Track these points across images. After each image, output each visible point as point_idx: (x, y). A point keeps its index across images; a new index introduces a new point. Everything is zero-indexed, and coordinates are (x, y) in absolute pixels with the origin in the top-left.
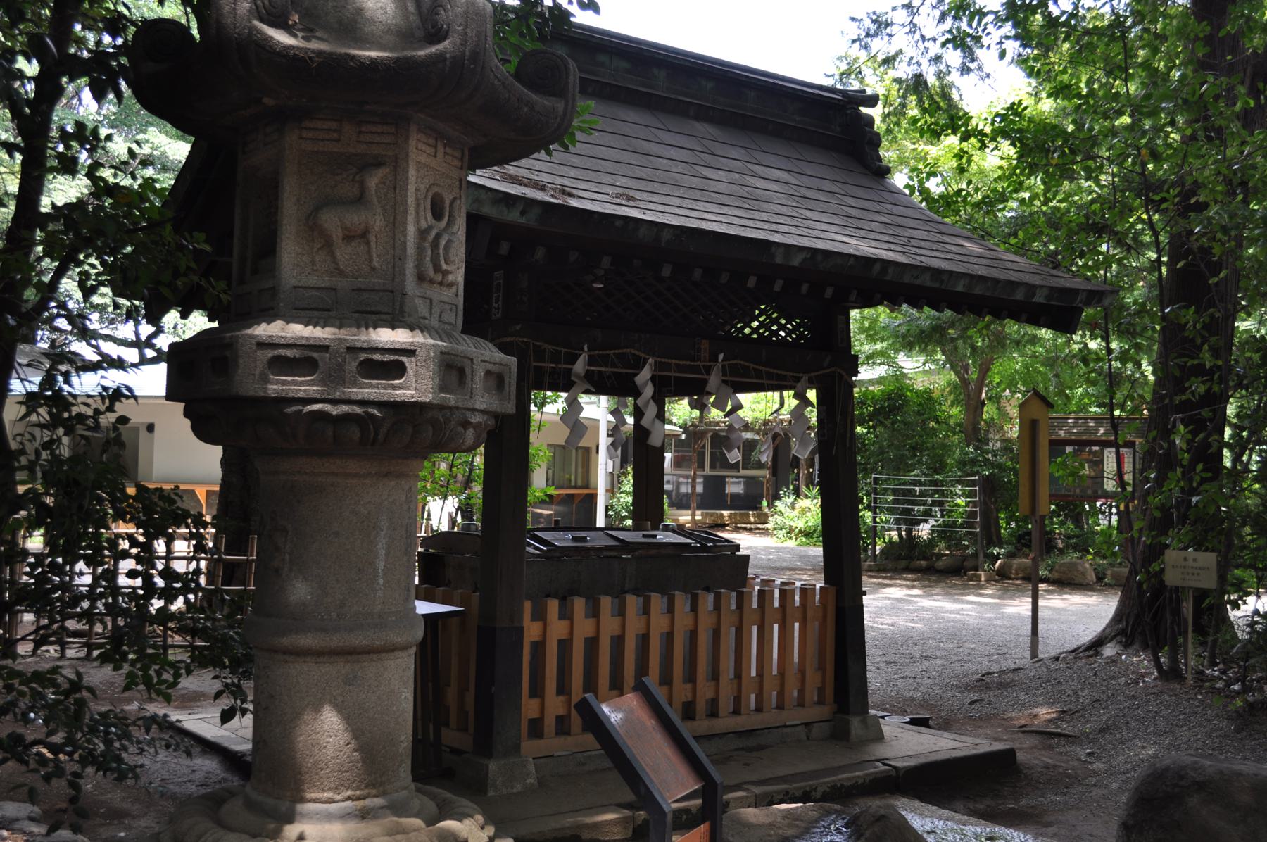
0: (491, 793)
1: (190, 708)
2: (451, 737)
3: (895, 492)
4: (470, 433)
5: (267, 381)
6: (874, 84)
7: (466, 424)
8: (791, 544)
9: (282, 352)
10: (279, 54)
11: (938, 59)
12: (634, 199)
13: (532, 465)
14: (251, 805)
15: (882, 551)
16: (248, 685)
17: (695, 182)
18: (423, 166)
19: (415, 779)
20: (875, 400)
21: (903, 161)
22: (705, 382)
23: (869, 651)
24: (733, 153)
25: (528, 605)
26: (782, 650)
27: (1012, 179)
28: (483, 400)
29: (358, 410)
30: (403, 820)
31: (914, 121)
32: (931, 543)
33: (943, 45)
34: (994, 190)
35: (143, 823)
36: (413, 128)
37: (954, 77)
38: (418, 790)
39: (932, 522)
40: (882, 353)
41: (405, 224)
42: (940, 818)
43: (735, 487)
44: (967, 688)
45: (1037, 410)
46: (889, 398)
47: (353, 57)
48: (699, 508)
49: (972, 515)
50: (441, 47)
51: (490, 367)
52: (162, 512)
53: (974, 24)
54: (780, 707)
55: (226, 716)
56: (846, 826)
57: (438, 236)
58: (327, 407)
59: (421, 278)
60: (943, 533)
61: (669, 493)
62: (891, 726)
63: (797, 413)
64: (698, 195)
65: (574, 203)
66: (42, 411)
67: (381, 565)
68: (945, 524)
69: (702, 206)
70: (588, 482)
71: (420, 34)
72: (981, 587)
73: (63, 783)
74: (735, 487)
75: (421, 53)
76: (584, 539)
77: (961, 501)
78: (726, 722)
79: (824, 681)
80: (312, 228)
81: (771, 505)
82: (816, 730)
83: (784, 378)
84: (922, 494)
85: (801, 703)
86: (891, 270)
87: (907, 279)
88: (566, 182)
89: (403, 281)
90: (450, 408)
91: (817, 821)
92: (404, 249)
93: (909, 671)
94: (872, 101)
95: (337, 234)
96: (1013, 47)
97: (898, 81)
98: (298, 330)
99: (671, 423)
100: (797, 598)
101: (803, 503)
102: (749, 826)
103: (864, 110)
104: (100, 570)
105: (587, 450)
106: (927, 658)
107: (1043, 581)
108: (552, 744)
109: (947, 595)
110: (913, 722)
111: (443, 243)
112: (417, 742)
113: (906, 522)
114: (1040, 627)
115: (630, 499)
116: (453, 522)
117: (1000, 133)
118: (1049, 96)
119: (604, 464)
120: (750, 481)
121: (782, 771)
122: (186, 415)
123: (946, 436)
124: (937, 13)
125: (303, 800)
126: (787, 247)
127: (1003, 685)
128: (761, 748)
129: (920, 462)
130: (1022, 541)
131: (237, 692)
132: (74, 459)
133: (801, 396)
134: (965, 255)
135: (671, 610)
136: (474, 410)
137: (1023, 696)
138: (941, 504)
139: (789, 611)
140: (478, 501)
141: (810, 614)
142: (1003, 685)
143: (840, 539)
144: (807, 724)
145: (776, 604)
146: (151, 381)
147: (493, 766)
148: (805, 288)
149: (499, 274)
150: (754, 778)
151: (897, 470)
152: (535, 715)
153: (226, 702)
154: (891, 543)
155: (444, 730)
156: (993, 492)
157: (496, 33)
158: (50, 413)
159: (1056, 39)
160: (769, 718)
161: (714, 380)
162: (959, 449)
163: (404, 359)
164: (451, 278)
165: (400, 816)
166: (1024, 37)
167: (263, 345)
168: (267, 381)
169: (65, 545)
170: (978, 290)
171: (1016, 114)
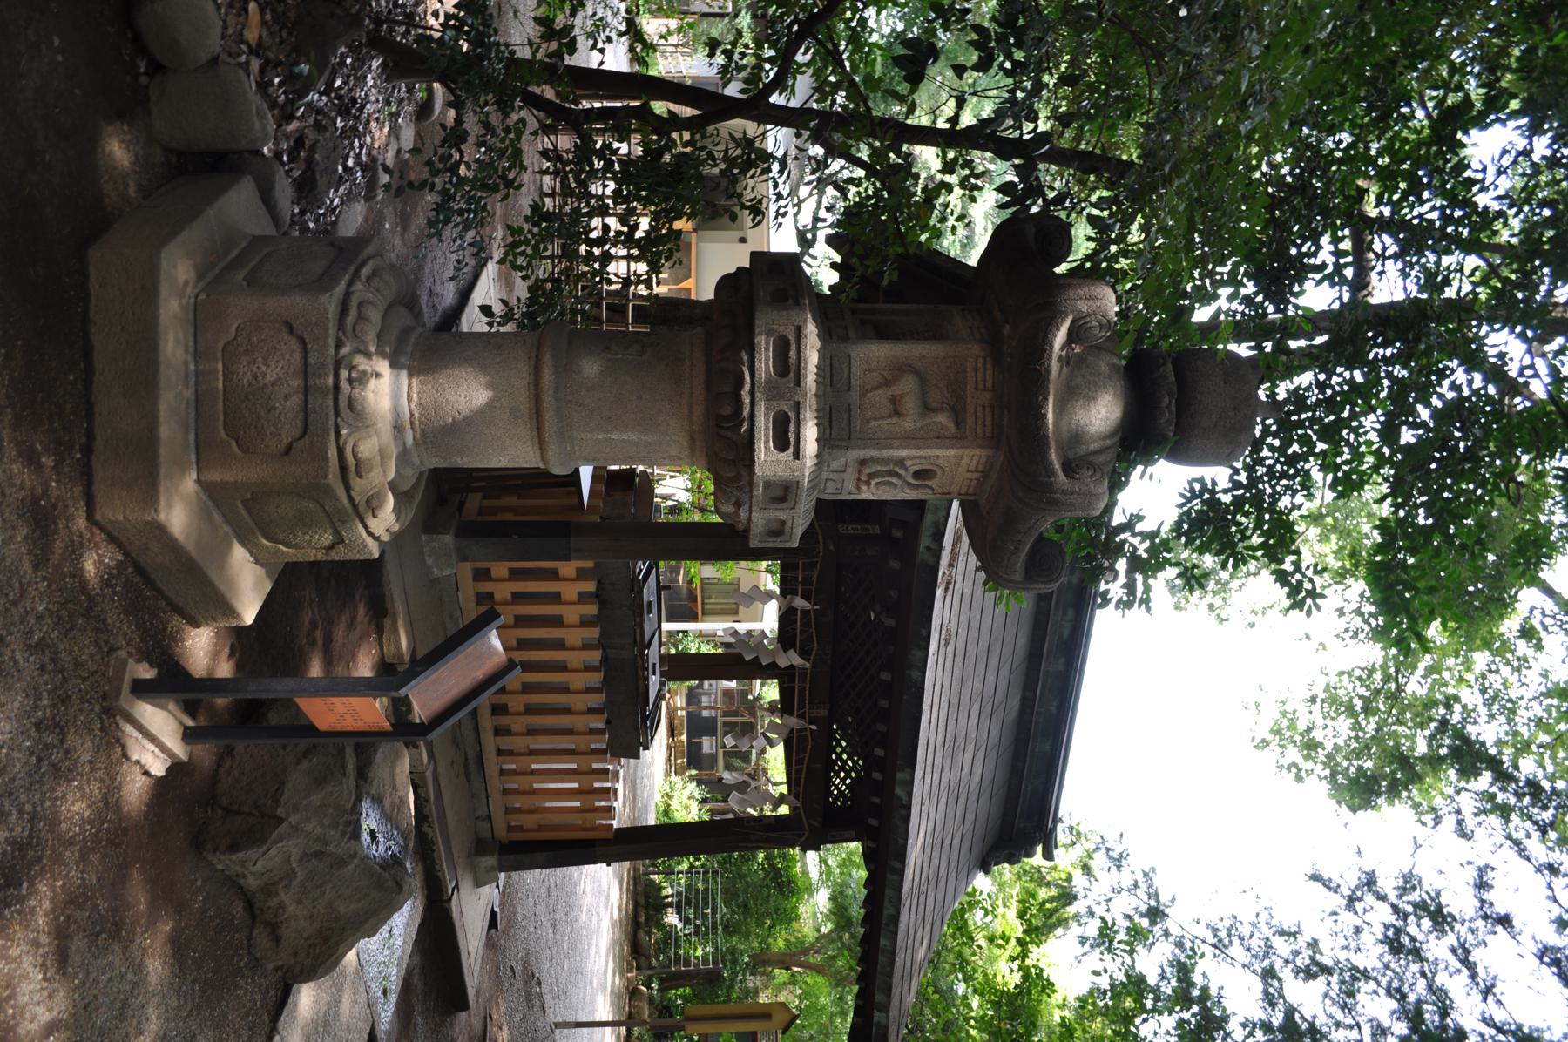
0: (424, 538)
1: (500, 280)
2: (474, 502)
3: (706, 890)
4: (730, 509)
5: (768, 335)
6: (1065, 858)
7: (738, 505)
8: (658, 798)
9: (793, 347)
10: (1046, 337)
11: (1092, 914)
12: (946, 644)
13: (718, 565)
14: (407, 332)
15: (653, 881)
16: (509, 328)
17: (966, 698)
18: (959, 462)
19: (435, 473)
20: (788, 868)
21: (1002, 886)
22: (791, 714)
23: (560, 871)
24: (994, 732)
25: (590, 564)
26: (554, 790)
27: (987, 989)
28: (759, 519)
29: (746, 412)
30: (393, 463)
31: (1033, 896)
32: (661, 925)
33: (1103, 919)
34: (975, 971)
35: (398, 242)
36: (991, 452)
37: (1075, 930)
38: (421, 474)
39: (680, 926)
40: (829, 872)
41: (907, 447)
42: (404, 942)
43: (707, 745)
44: (526, 963)
45: (779, 1019)
46: (790, 882)
47: (1046, 399)
48: (689, 713)
49: (687, 963)
50: (1060, 473)
51: (789, 524)
52: (660, 249)
53: (1122, 946)
54: (505, 792)
55: (486, 310)
56: (393, 855)
57: (899, 476)
58: (747, 386)
59: (863, 463)
60: (670, 936)
61: (700, 686)
62: (489, 895)
63: (767, 796)
64: (954, 701)
65: (939, 593)
66: (739, 151)
67: (614, 436)
68: (677, 938)
69: (944, 705)
70: (707, 614)
71: (1070, 455)
72: (621, 973)
73: (426, 175)
74: (707, 745)
75: (1054, 456)
76: (650, 611)
77: (699, 952)
78: (490, 743)
79: (528, 830)
80: (901, 369)
81: (692, 778)
82: (486, 825)
83: (798, 784)
84: (705, 916)
85: (508, 810)
86: (895, 877)
87: (889, 893)
88: (958, 585)
89: (859, 447)
90: (751, 491)
91: (397, 828)
92: (891, 447)
93: (541, 909)
94: (1048, 855)
95: (894, 391)
96: (1104, 982)
97: (1069, 879)
98: (812, 358)
99: (763, 685)
100: (603, 803)
101: (694, 807)
102: (393, 767)
103: (1039, 849)
104: (610, 202)
105: (736, 613)
106: (554, 926)
107: (628, 1031)
108: (468, 590)
109: (614, 942)
110: (493, 915)
111: (894, 480)
112: (471, 473)
113: (680, 901)
114: (585, 1030)
115: (693, 651)
116: (665, 498)
117: (1026, 976)
118: (1063, 1018)
119: (718, 626)
120: (713, 758)
121: (446, 797)
122: (740, 269)
123: (757, 936)
124: (1132, 913)
125: (410, 376)
126: (912, 783)
127: (529, 998)
128: (468, 775)
129: (733, 912)
130: (664, 1010)
131: (508, 317)
132: (700, 178)
133: (781, 800)
134: (914, 944)
135: (589, 690)
136: (750, 511)
137: (518, 1016)
138: (696, 933)
139: (591, 797)
140: (684, 518)
141: (588, 815)
142: (529, 998)
143: (667, 839)
144: (489, 817)
145: (596, 785)
146: (782, 241)
147: (448, 539)
148: (877, 800)
149: (877, 529)
150: (440, 770)
151: (725, 891)
152: (494, 573)
153: (498, 309)
154: (661, 888)
155: (480, 495)
156: (709, 981)
157: (1078, 520)
158: (737, 157)
159: (1114, 1022)
160: (495, 783)
161: (793, 721)
162: (746, 948)
163: (791, 450)
164: (864, 488)
165: (398, 458)
166: (1117, 991)
167: (799, 330)
168: (769, 334)
169: (629, 173)
170: (881, 958)
171: (1044, 987)
